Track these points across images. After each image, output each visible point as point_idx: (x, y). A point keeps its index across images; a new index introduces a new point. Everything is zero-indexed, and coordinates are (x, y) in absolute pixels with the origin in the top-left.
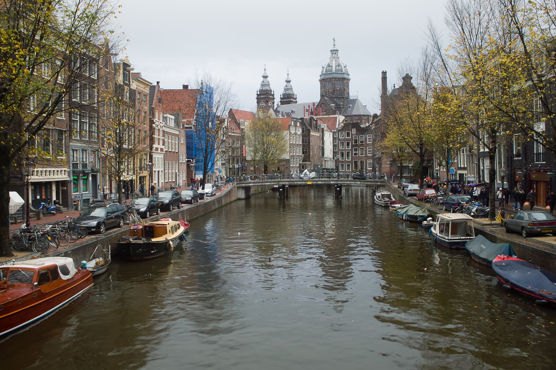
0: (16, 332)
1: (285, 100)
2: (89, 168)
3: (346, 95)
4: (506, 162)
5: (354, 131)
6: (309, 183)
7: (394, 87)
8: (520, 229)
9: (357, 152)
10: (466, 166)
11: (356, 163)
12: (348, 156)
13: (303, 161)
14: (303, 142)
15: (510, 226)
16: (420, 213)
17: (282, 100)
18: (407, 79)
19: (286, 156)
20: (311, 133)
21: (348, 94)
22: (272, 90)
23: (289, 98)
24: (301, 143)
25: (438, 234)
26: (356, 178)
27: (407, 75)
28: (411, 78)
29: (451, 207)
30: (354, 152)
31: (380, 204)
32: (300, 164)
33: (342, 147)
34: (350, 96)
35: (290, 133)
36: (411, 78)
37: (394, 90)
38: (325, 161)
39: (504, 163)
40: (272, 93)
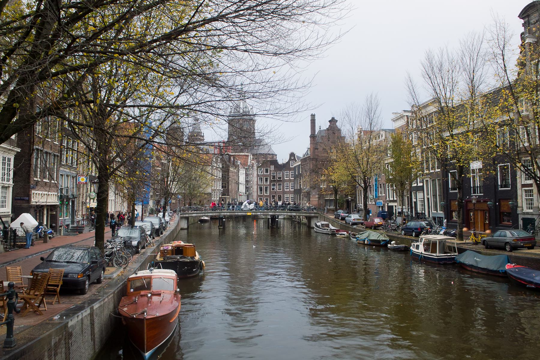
2: (70, 193)
4: (442, 194)
5: (272, 167)
6: (249, 214)
7: (320, 128)
8: (503, 244)
9: (275, 187)
10: (395, 199)
12: (266, 191)
13: (222, 195)
15: (490, 243)
16: (382, 238)
18: (333, 121)
19: (209, 190)
25: (423, 252)
26: (292, 210)
28: (337, 121)
29: (413, 231)
30: (272, 187)
32: (220, 198)
33: (260, 182)
36: (337, 121)
37: (320, 131)
38: (240, 195)
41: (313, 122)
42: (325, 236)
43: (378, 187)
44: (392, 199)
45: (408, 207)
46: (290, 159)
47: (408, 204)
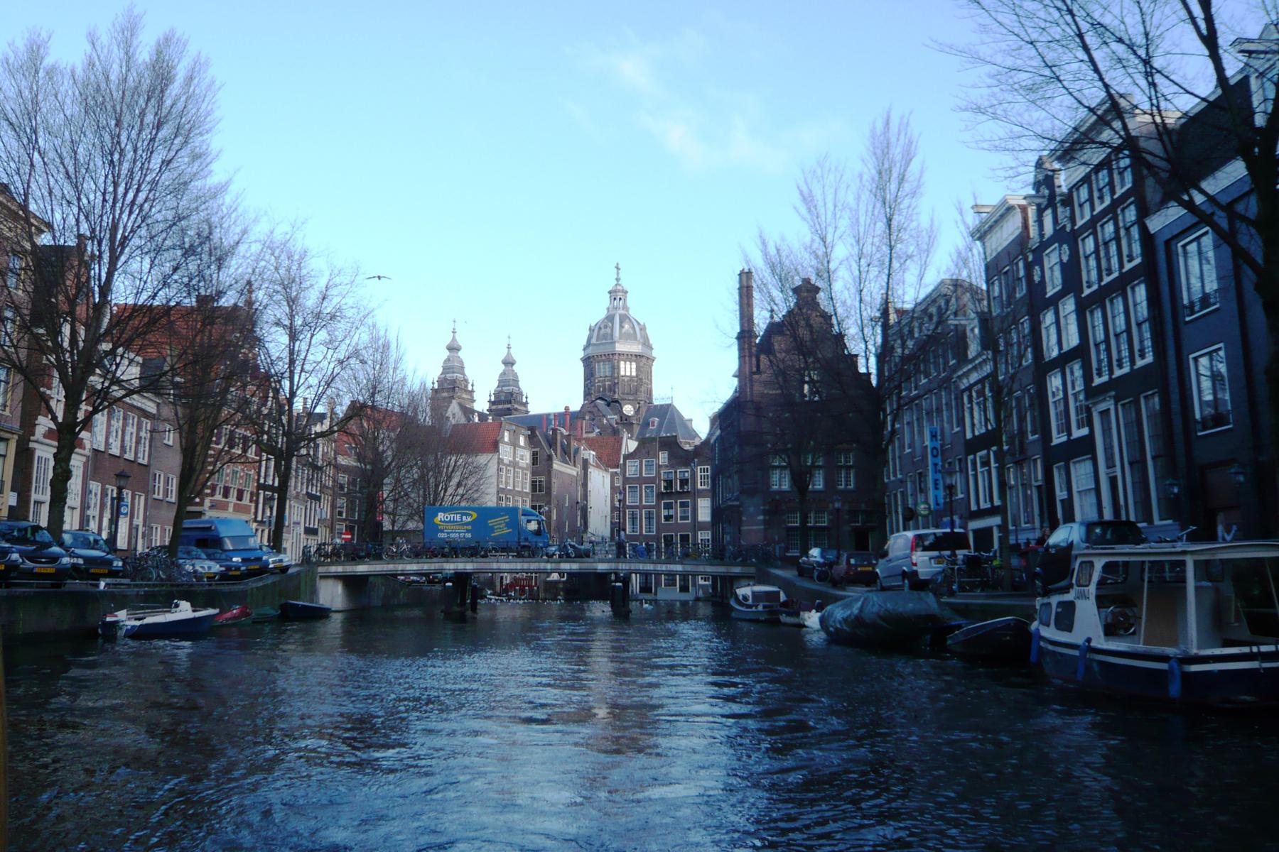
1: (500, 407)
3: (643, 395)
5: (663, 457)
10: (997, 502)
11: (669, 541)
17: (494, 407)
20: (555, 466)
21: (649, 392)
22: (470, 381)
23: (510, 402)
24: (528, 489)
25: (1100, 642)
27: (807, 281)
30: (664, 513)
31: (751, 617)
34: (654, 397)
35: (500, 461)
39: (1154, 458)
40: (470, 388)
44: (988, 505)
47: (1041, 515)
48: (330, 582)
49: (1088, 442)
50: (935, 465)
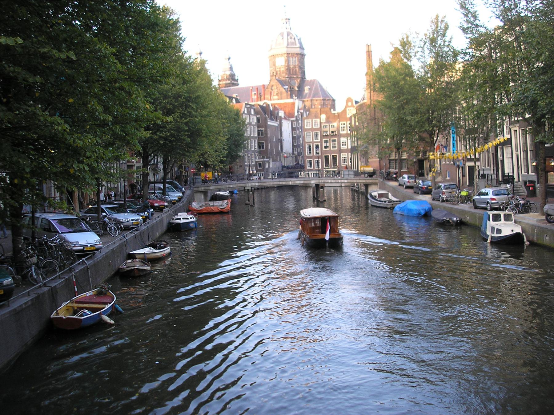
0: (212, 387)
9: (328, 144)
14: (259, 134)
20: (269, 123)
21: (303, 73)
24: (256, 135)
32: (256, 162)
38: (284, 157)
39: (530, 151)
41: (369, 53)
42: (383, 210)
43: (456, 141)
45: (493, 167)
46: (347, 106)
47: (493, 164)
48: (199, 194)
49: (510, 140)
50: (453, 137)
